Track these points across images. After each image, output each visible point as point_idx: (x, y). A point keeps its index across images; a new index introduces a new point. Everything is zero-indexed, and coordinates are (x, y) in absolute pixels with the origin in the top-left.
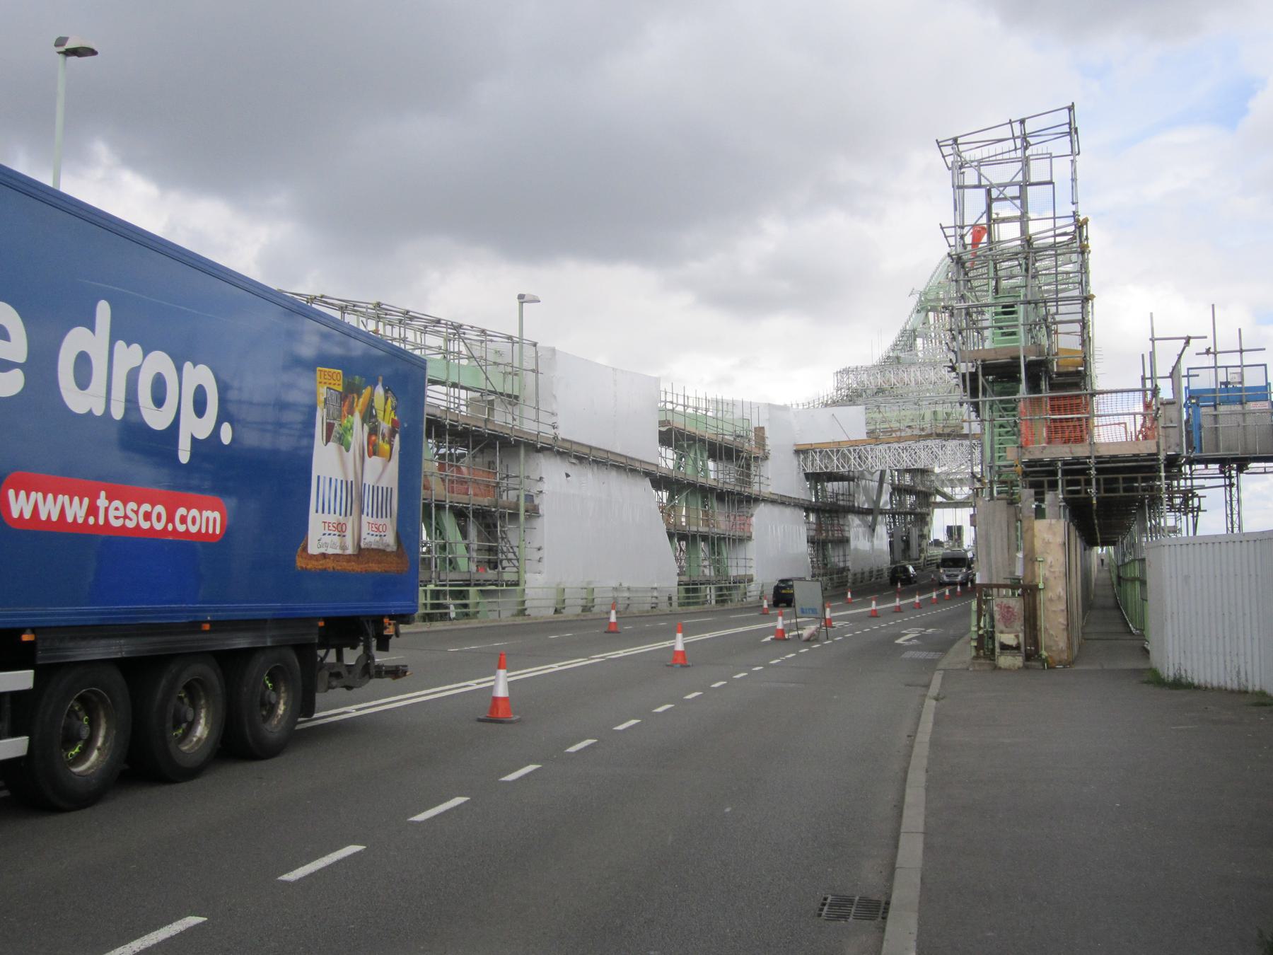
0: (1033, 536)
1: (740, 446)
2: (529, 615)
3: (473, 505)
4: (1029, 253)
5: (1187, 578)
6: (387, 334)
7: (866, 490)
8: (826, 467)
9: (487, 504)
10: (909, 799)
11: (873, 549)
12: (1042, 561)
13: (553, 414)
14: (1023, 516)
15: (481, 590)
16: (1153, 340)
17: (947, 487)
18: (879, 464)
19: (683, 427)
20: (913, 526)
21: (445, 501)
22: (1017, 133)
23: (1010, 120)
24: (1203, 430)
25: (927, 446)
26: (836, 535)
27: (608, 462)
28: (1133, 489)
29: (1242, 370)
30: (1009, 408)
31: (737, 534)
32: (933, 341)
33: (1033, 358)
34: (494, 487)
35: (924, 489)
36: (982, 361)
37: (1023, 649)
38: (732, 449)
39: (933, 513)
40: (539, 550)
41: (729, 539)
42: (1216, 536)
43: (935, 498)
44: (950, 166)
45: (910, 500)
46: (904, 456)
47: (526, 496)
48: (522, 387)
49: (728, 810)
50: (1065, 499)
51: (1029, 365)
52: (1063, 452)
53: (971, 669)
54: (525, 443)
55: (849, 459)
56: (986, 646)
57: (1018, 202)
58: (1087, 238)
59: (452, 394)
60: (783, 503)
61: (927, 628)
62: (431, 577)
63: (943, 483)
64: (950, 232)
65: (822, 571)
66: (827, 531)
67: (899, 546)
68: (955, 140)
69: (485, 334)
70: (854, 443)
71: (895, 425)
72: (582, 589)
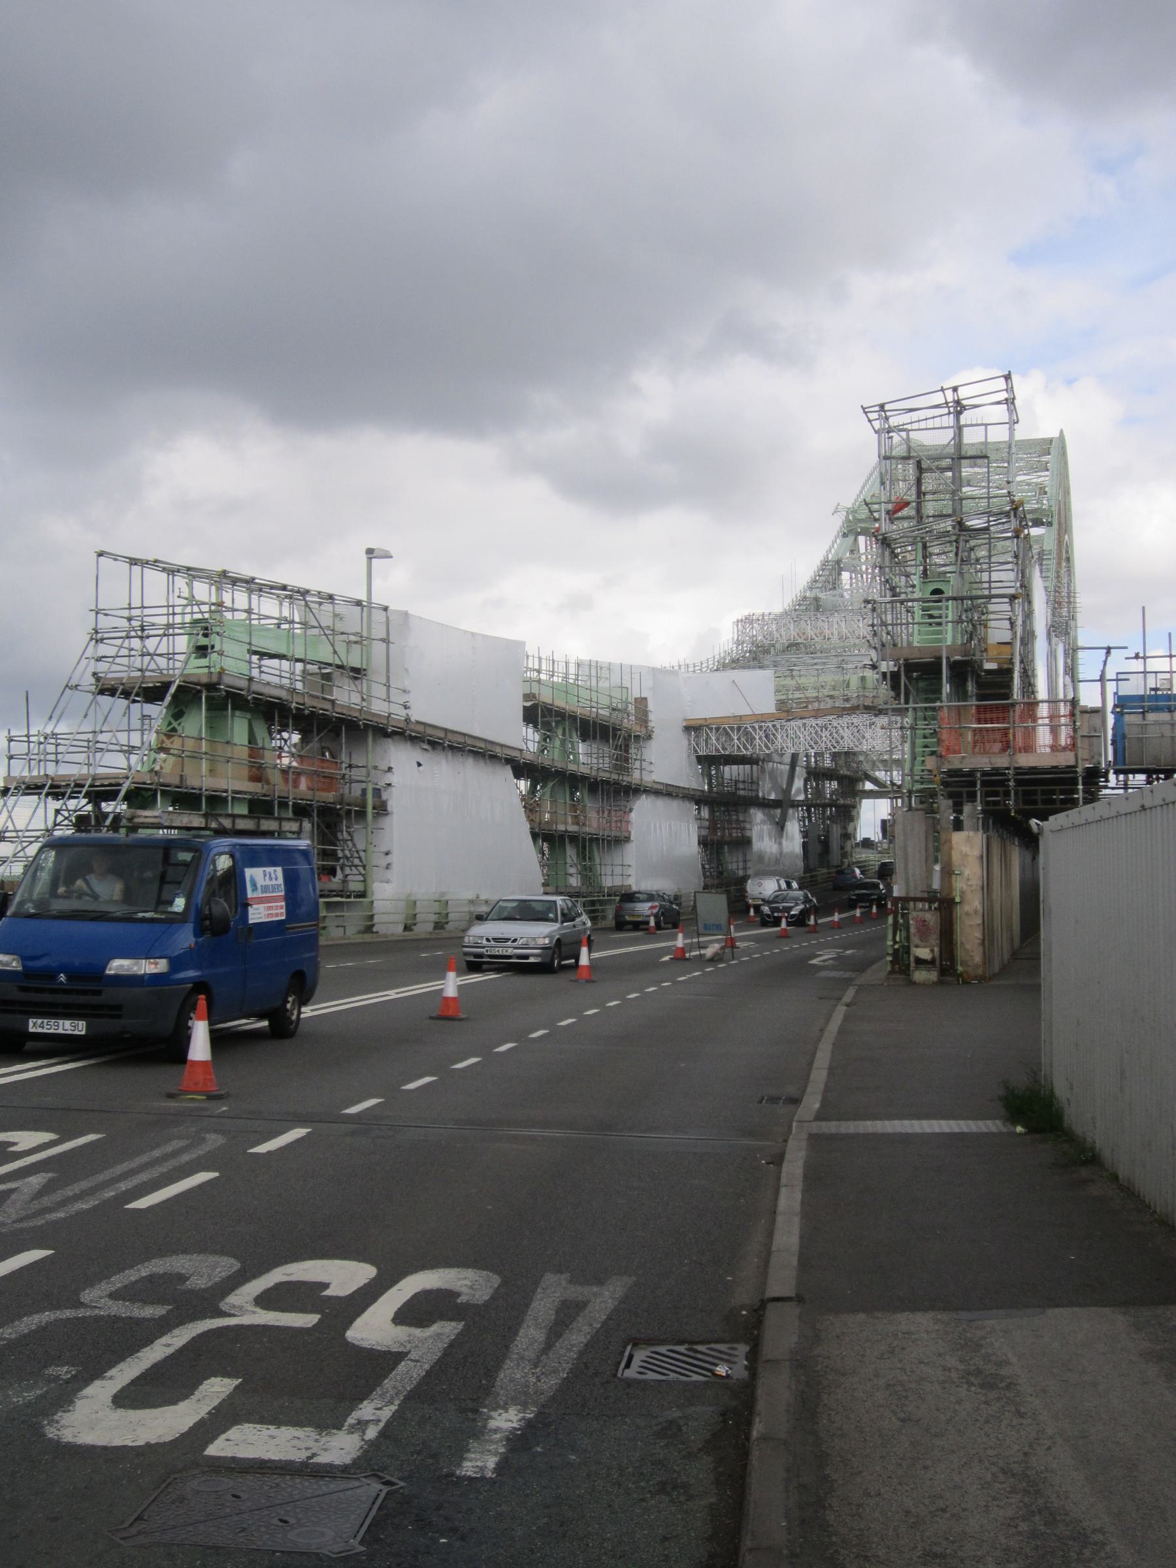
0: (951, 848)
1: (618, 722)
2: (377, 932)
3: (318, 801)
4: (960, 535)
7: (773, 775)
8: (724, 749)
9: (332, 801)
11: (781, 853)
13: (404, 691)
17: (879, 770)
20: (832, 822)
21: (288, 798)
23: (942, 387)
24: (1126, 741)
25: (852, 724)
26: (734, 835)
29: (1171, 676)
31: (613, 834)
32: (864, 576)
33: (958, 658)
35: (849, 773)
36: (905, 660)
39: (860, 805)
40: (387, 854)
41: (603, 840)
43: (864, 785)
45: (831, 786)
46: (824, 735)
47: (374, 789)
50: (983, 811)
51: (953, 666)
53: (885, 984)
60: (669, 795)
61: (847, 949)
65: (716, 882)
66: (723, 829)
67: (816, 848)
70: (760, 718)
71: (811, 694)
72: (436, 901)
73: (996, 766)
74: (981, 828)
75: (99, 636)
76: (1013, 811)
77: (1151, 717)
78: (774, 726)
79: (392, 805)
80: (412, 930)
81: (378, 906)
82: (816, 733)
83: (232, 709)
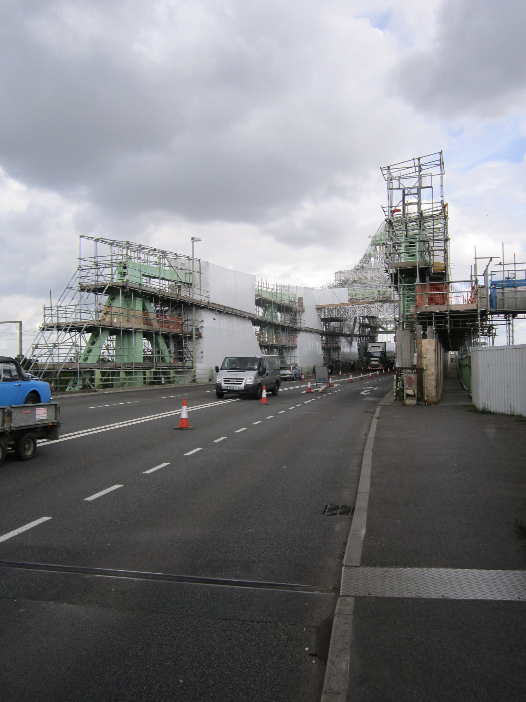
0: (422, 346)
1: (292, 306)
2: (197, 382)
3: (172, 333)
5: (489, 365)
7: (348, 326)
9: (178, 333)
10: (364, 462)
17: (384, 324)
18: (354, 314)
19: (266, 298)
21: (159, 331)
26: (335, 346)
27: (208, 307)
29: (515, 272)
32: (379, 259)
33: (422, 266)
36: (400, 268)
37: (416, 396)
40: (202, 353)
41: (287, 347)
42: (502, 346)
43: (379, 329)
44: (386, 179)
45: (368, 330)
46: (365, 310)
48: (194, 280)
50: (436, 330)
51: (421, 270)
53: (393, 405)
54: (195, 305)
55: (341, 312)
57: (416, 196)
58: (447, 213)
59: (162, 283)
63: (382, 323)
66: (331, 344)
68: (389, 167)
70: (343, 305)
71: (361, 297)
74: (434, 337)
75: (81, 268)
76: (449, 330)
77: (506, 290)
78: (348, 307)
79: (203, 335)
83: (133, 297)
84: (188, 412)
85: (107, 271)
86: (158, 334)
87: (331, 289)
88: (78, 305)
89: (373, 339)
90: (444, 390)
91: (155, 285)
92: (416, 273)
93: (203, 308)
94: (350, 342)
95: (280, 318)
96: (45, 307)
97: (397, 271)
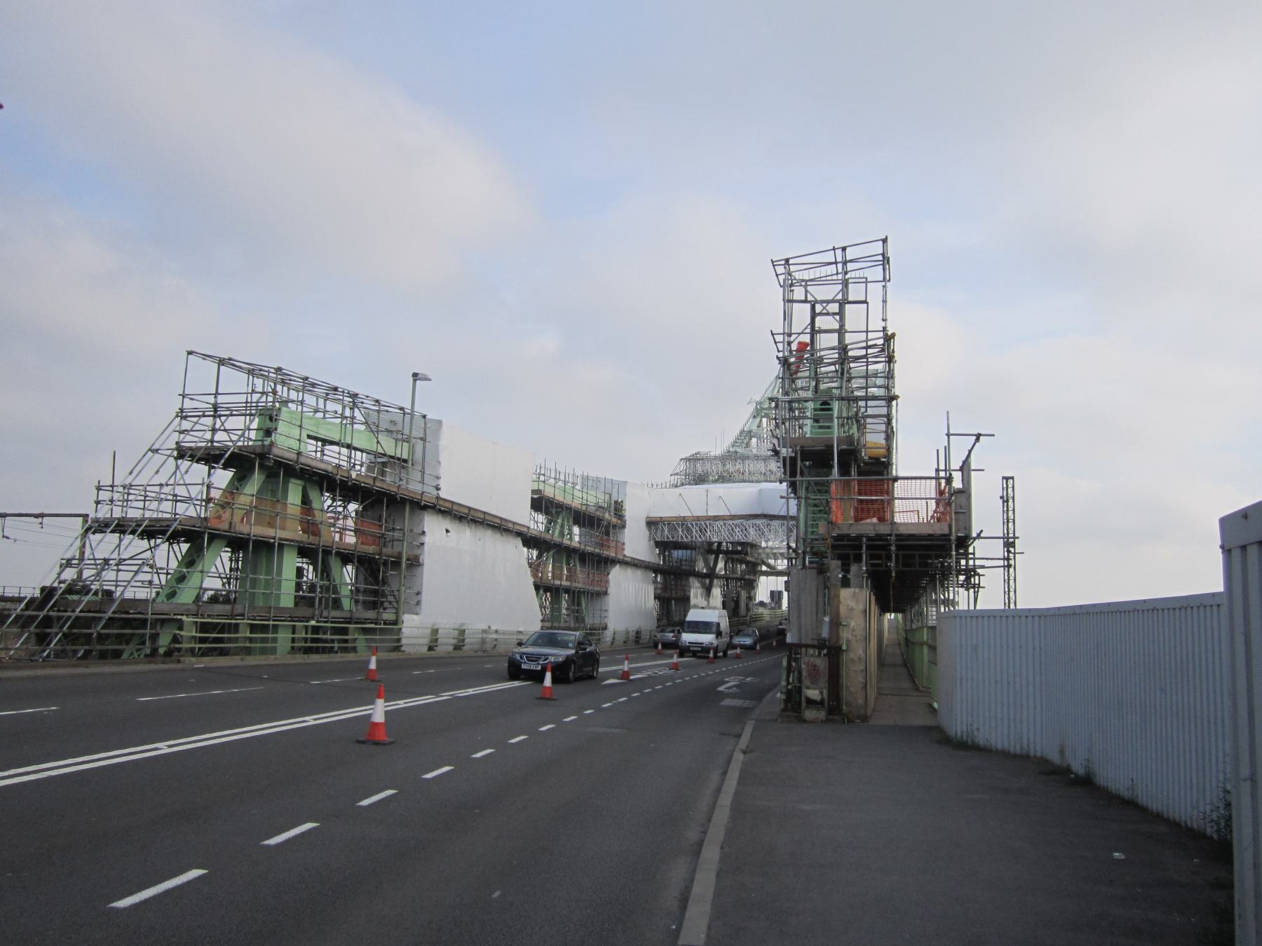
0: (839, 602)
2: (404, 651)
3: (358, 552)
5: (975, 648)
6: (284, 395)
9: (372, 552)
10: (696, 889)
12: (846, 625)
13: (437, 478)
14: (831, 585)
15: (362, 628)
16: (948, 435)
17: (771, 558)
19: (553, 496)
20: (742, 589)
21: (332, 547)
22: (839, 259)
23: (834, 247)
27: (436, 506)
28: (927, 565)
30: (823, 488)
32: (765, 441)
33: (845, 447)
34: (380, 537)
36: (801, 447)
37: (826, 705)
38: (594, 517)
40: (418, 594)
41: (588, 593)
42: (1030, 610)
43: (761, 568)
44: (782, 284)
45: (741, 568)
46: (737, 531)
48: (412, 451)
49: (496, 894)
52: (870, 525)
56: (794, 703)
57: (837, 317)
58: (893, 351)
61: (747, 677)
62: (314, 615)
63: (768, 556)
64: (779, 338)
68: (787, 261)
69: (379, 403)
70: (696, 518)
73: (878, 532)
76: (894, 572)
80: (435, 650)
81: (406, 631)
82: (733, 529)
84: (385, 711)
85: (236, 423)
86: (329, 553)
87: (677, 489)
88: (167, 485)
89: (749, 586)
90: (879, 688)
91: (334, 457)
92: (833, 459)
93: (425, 508)
94: (707, 588)
95: (576, 536)
96: (101, 484)
97: (796, 454)
